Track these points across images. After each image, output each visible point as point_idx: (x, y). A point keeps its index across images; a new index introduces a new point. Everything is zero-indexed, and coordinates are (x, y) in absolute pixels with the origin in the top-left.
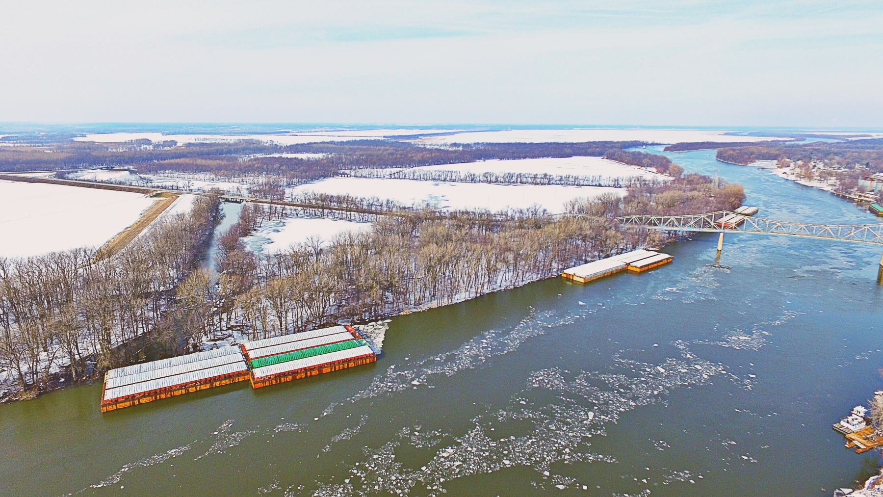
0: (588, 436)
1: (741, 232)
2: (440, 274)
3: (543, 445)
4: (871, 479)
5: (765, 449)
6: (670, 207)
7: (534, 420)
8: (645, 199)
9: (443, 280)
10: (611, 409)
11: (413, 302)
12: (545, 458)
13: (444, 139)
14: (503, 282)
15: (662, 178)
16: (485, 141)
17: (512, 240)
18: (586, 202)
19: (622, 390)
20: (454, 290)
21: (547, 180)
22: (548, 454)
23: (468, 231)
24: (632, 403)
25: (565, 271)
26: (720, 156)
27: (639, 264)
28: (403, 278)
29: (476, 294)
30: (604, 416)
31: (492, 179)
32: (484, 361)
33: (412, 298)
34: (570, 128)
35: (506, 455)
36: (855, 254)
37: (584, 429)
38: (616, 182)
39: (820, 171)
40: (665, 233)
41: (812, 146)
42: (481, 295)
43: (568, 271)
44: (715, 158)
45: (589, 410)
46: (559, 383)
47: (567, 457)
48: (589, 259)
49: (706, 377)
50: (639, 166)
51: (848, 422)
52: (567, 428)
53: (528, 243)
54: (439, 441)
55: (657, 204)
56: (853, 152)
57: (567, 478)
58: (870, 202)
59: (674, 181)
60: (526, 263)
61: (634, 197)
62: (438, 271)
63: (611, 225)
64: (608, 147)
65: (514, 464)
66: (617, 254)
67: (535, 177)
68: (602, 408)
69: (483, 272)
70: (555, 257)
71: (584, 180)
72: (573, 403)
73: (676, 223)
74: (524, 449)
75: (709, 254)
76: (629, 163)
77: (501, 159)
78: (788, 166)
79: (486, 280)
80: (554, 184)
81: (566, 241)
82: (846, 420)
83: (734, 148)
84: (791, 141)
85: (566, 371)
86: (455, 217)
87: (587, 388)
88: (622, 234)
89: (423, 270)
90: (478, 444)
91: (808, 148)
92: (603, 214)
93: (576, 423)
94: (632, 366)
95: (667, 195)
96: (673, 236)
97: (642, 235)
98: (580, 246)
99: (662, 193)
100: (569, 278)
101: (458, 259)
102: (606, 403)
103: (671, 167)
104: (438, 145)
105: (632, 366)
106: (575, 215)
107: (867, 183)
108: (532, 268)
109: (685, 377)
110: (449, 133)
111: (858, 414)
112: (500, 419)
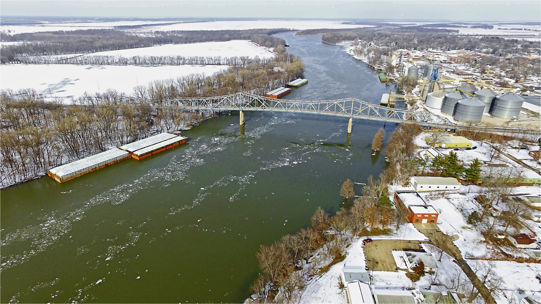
16: (179, 30)
27: (139, 153)
34: (255, 19)
84: (373, 28)
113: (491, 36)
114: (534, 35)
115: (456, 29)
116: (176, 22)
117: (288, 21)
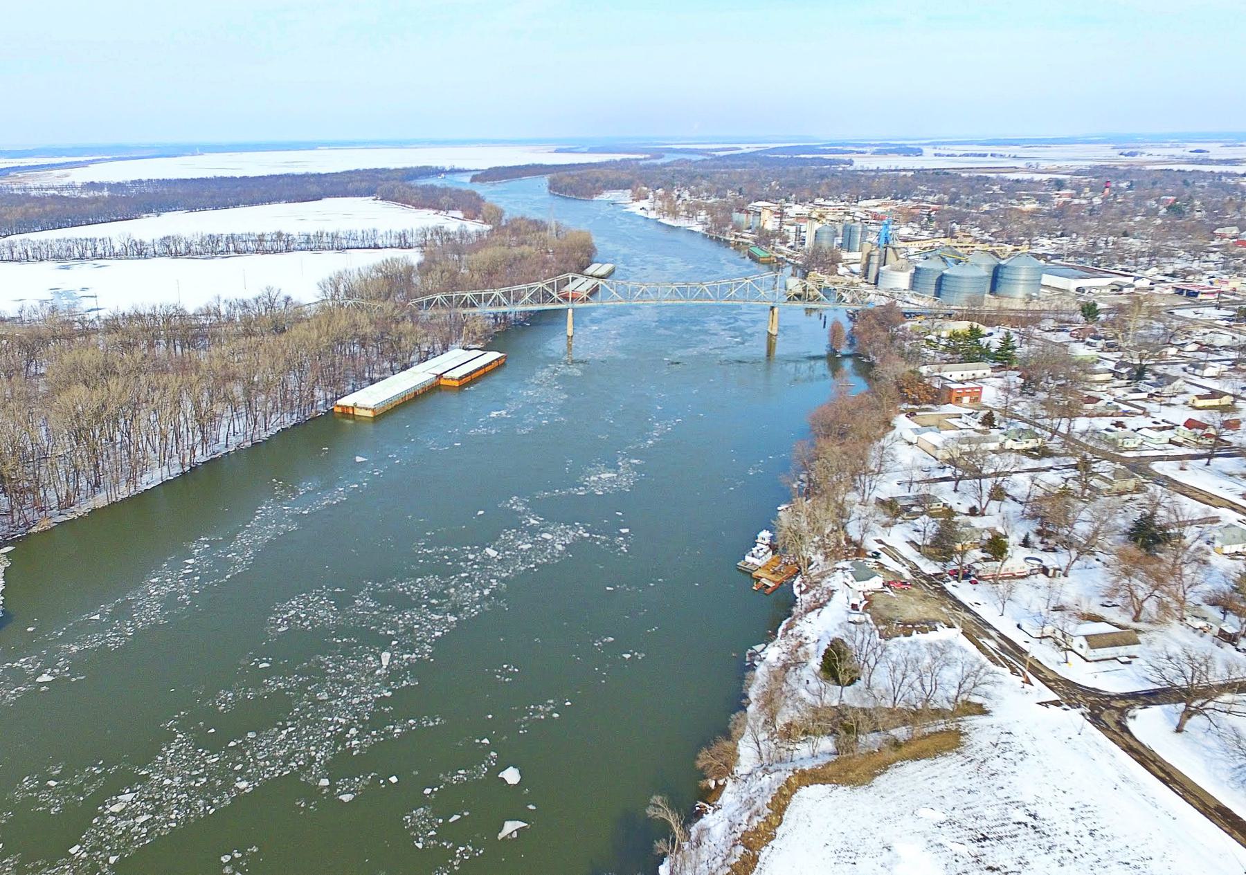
0: (386, 694)
1: (595, 304)
2: (103, 440)
3: (307, 735)
4: (783, 626)
5: (653, 632)
6: (491, 275)
7: (291, 690)
8: (451, 266)
9: (111, 451)
10: (420, 638)
11: (56, 505)
12: (314, 757)
13: (67, 176)
14: (231, 438)
15: (473, 227)
16: (154, 177)
17: (236, 359)
18: (357, 277)
19: (434, 601)
20: (137, 467)
21: (282, 244)
22: (317, 748)
23: (146, 352)
24: (452, 619)
25: (340, 402)
26: (555, 188)
27: (457, 374)
28: (25, 460)
29: (183, 468)
30: (408, 653)
31: (178, 248)
32: (188, 603)
33: (52, 496)
34: (311, 146)
35: (241, 772)
36: (737, 324)
37: (377, 684)
38: (402, 239)
39: (686, 203)
40: (489, 318)
41: (673, 166)
42: (191, 468)
43: (346, 401)
44: (546, 190)
45: (383, 651)
46: (326, 614)
47: (355, 742)
48: (376, 376)
49: (560, 547)
50: (436, 209)
51: (753, 556)
52: (348, 690)
53: (266, 361)
54: (100, 782)
55: (470, 270)
56: (722, 173)
57: (357, 780)
58: (748, 244)
59: (492, 231)
60: (267, 399)
61: (434, 262)
62: (97, 437)
63: (403, 314)
64: (382, 180)
65: (256, 784)
66: (421, 361)
67: (261, 239)
68: (404, 641)
69: (190, 425)
70: (317, 380)
71: (348, 239)
72: (354, 644)
73: (504, 300)
74: (274, 751)
75: (556, 345)
76: (419, 206)
77: (191, 209)
78: (647, 198)
79: (198, 439)
80: (297, 250)
81: (333, 350)
82: (750, 553)
83: (572, 172)
84: (645, 159)
85: (338, 590)
86: (116, 328)
87: (375, 613)
88: (423, 328)
89: (66, 438)
90: (184, 768)
91: (667, 169)
92: (387, 296)
93: (363, 678)
94: (446, 557)
95: (485, 255)
96: (503, 321)
97: (454, 326)
98: (358, 355)
99: (476, 252)
100: (347, 413)
101: (135, 406)
102: (409, 630)
103: (484, 208)
104: (56, 189)
105: (446, 557)
106: (341, 302)
107: (743, 217)
108: (280, 405)
109: (529, 557)
110: (76, 162)
111: (764, 542)
112: (221, 708)
113: (932, 172)
114: (1015, 168)
115: (846, 157)
116: (92, 158)
117: (403, 148)
